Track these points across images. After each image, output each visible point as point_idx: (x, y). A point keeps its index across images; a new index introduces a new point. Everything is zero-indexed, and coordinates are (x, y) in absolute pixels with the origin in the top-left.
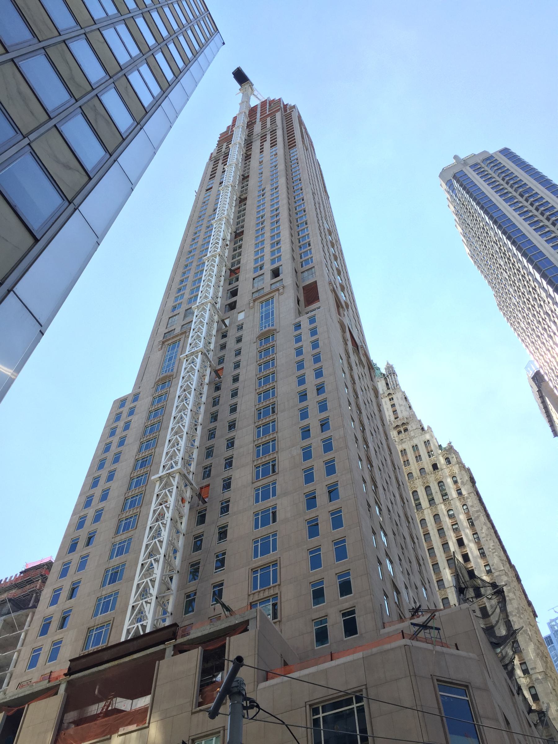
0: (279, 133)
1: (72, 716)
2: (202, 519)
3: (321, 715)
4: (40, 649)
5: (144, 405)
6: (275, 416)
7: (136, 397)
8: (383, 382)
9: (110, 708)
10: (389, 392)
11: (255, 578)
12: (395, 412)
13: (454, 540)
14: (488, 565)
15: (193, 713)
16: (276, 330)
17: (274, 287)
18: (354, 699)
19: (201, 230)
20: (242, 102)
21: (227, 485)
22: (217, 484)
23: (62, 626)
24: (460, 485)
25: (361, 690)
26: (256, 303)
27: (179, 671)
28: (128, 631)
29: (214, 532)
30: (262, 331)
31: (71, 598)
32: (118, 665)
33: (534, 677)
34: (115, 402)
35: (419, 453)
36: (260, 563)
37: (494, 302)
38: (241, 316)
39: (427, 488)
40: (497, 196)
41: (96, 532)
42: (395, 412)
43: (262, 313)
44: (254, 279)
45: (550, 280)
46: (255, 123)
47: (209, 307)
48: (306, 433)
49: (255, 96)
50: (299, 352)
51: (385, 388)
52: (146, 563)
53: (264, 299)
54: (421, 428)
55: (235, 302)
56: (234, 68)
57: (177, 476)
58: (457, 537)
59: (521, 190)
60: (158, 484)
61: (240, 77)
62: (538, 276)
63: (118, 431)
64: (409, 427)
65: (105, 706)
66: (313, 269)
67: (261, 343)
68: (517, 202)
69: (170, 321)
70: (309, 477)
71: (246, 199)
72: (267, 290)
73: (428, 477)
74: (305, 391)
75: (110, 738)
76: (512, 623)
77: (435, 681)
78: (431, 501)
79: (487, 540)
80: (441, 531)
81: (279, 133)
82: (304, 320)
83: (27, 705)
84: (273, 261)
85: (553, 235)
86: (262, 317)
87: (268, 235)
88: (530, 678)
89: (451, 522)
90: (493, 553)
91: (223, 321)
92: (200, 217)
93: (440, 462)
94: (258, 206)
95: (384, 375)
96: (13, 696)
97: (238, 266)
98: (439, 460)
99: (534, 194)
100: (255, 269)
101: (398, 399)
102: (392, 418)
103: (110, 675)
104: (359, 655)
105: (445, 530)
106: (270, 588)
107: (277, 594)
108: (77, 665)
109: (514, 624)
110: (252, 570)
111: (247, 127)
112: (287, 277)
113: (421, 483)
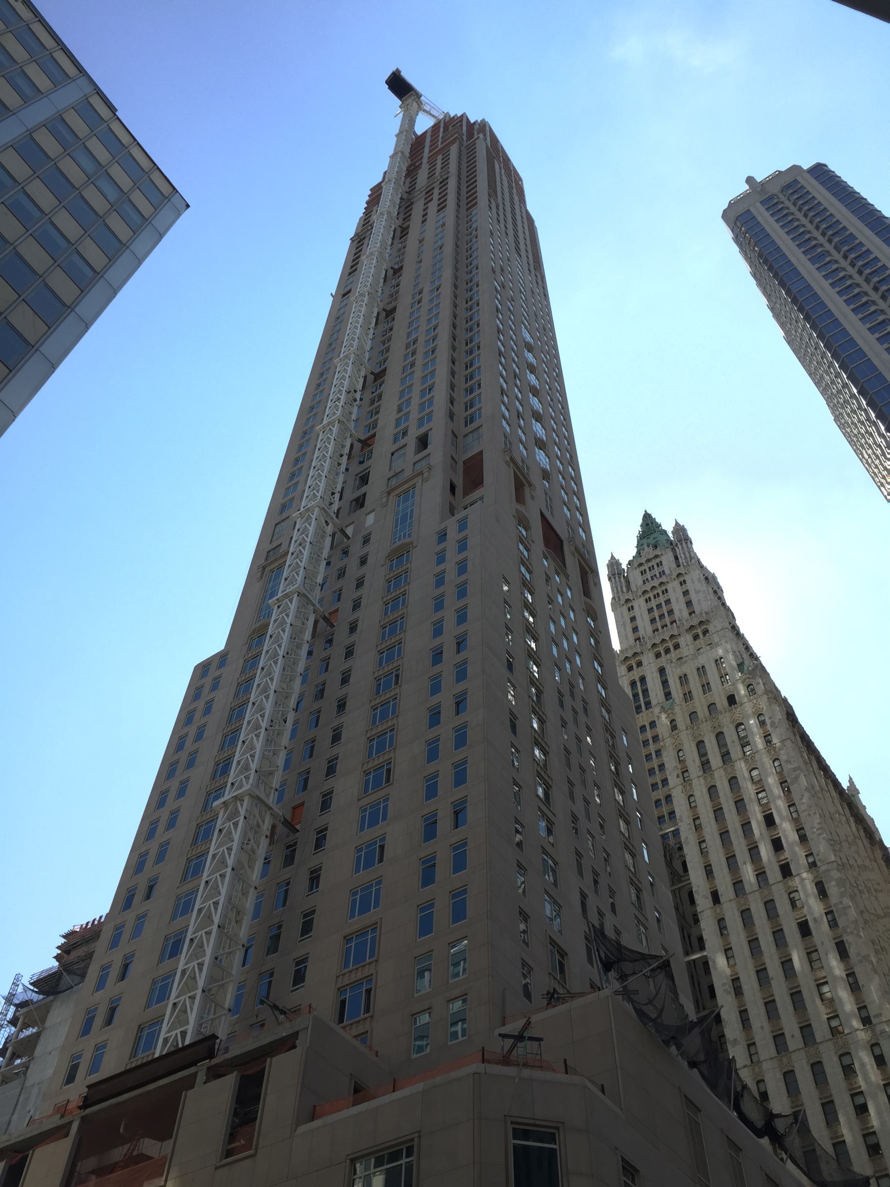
0: (452, 184)
1: (89, 1164)
2: (289, 860)
5: (231, 674)
7: (221, 658)
8: (670, 555)
9: (135, 1153)
11: (348, 950)
12: (689, 603)
13: (760, 817)
15: (216, 1168)
16: (412, 543)
20: (401, 132)
22: (314, 800)
23: (109, 1021)
24: (769, 727)
25: (412, 1140)
26: (391, 497)
27: (208, 1103)
28: (166, 1040)
29: (303, 878)
33: (878, 1028)
35: (707, 678)
38: (370, 520)
39: (720, 736)
40: (799, 252)
41: (157, 878)
42: (689, 603)
43: (397, 514)
44: (392, 454)
45: (871, 398)
48: (435, 717)
50: (440, 581)
51: (674, 565)
53: (402, 489)
56: (387, 74)
57: (246, 800)
59: (836, 239)
61: (399, 85)
63: (197, 715)
64: (711, 628)
65: (129, 1150)
67: (391, 566)
68: (830, 262)
69: (277, 530)
70: (431, 791)
71: (394, 310)
72: (408, 473)
74: (441, 646)
76: (847, 946)
78: (726, 756)
79: (809, 815)
80: (740, 804)
81: (452, 184)
82: (452, 525)
83: (31, 1152)
85: (881, 318)
86: (397, 520)
87: (418, 373)
88: (873, 1031)
89: (755, 788)
90: (819, 834)
91: (343, 532)
93: (738, 693)
95: (671, 543)
97: (373, 431)
98: (737, 689)
99: (857, 244)
101: (693, 582)
102: (685, 613)
104: (419, 1087)
105: (746, 801)
108: (98, 1093)
110: (345, 937)
111: (407, 176)
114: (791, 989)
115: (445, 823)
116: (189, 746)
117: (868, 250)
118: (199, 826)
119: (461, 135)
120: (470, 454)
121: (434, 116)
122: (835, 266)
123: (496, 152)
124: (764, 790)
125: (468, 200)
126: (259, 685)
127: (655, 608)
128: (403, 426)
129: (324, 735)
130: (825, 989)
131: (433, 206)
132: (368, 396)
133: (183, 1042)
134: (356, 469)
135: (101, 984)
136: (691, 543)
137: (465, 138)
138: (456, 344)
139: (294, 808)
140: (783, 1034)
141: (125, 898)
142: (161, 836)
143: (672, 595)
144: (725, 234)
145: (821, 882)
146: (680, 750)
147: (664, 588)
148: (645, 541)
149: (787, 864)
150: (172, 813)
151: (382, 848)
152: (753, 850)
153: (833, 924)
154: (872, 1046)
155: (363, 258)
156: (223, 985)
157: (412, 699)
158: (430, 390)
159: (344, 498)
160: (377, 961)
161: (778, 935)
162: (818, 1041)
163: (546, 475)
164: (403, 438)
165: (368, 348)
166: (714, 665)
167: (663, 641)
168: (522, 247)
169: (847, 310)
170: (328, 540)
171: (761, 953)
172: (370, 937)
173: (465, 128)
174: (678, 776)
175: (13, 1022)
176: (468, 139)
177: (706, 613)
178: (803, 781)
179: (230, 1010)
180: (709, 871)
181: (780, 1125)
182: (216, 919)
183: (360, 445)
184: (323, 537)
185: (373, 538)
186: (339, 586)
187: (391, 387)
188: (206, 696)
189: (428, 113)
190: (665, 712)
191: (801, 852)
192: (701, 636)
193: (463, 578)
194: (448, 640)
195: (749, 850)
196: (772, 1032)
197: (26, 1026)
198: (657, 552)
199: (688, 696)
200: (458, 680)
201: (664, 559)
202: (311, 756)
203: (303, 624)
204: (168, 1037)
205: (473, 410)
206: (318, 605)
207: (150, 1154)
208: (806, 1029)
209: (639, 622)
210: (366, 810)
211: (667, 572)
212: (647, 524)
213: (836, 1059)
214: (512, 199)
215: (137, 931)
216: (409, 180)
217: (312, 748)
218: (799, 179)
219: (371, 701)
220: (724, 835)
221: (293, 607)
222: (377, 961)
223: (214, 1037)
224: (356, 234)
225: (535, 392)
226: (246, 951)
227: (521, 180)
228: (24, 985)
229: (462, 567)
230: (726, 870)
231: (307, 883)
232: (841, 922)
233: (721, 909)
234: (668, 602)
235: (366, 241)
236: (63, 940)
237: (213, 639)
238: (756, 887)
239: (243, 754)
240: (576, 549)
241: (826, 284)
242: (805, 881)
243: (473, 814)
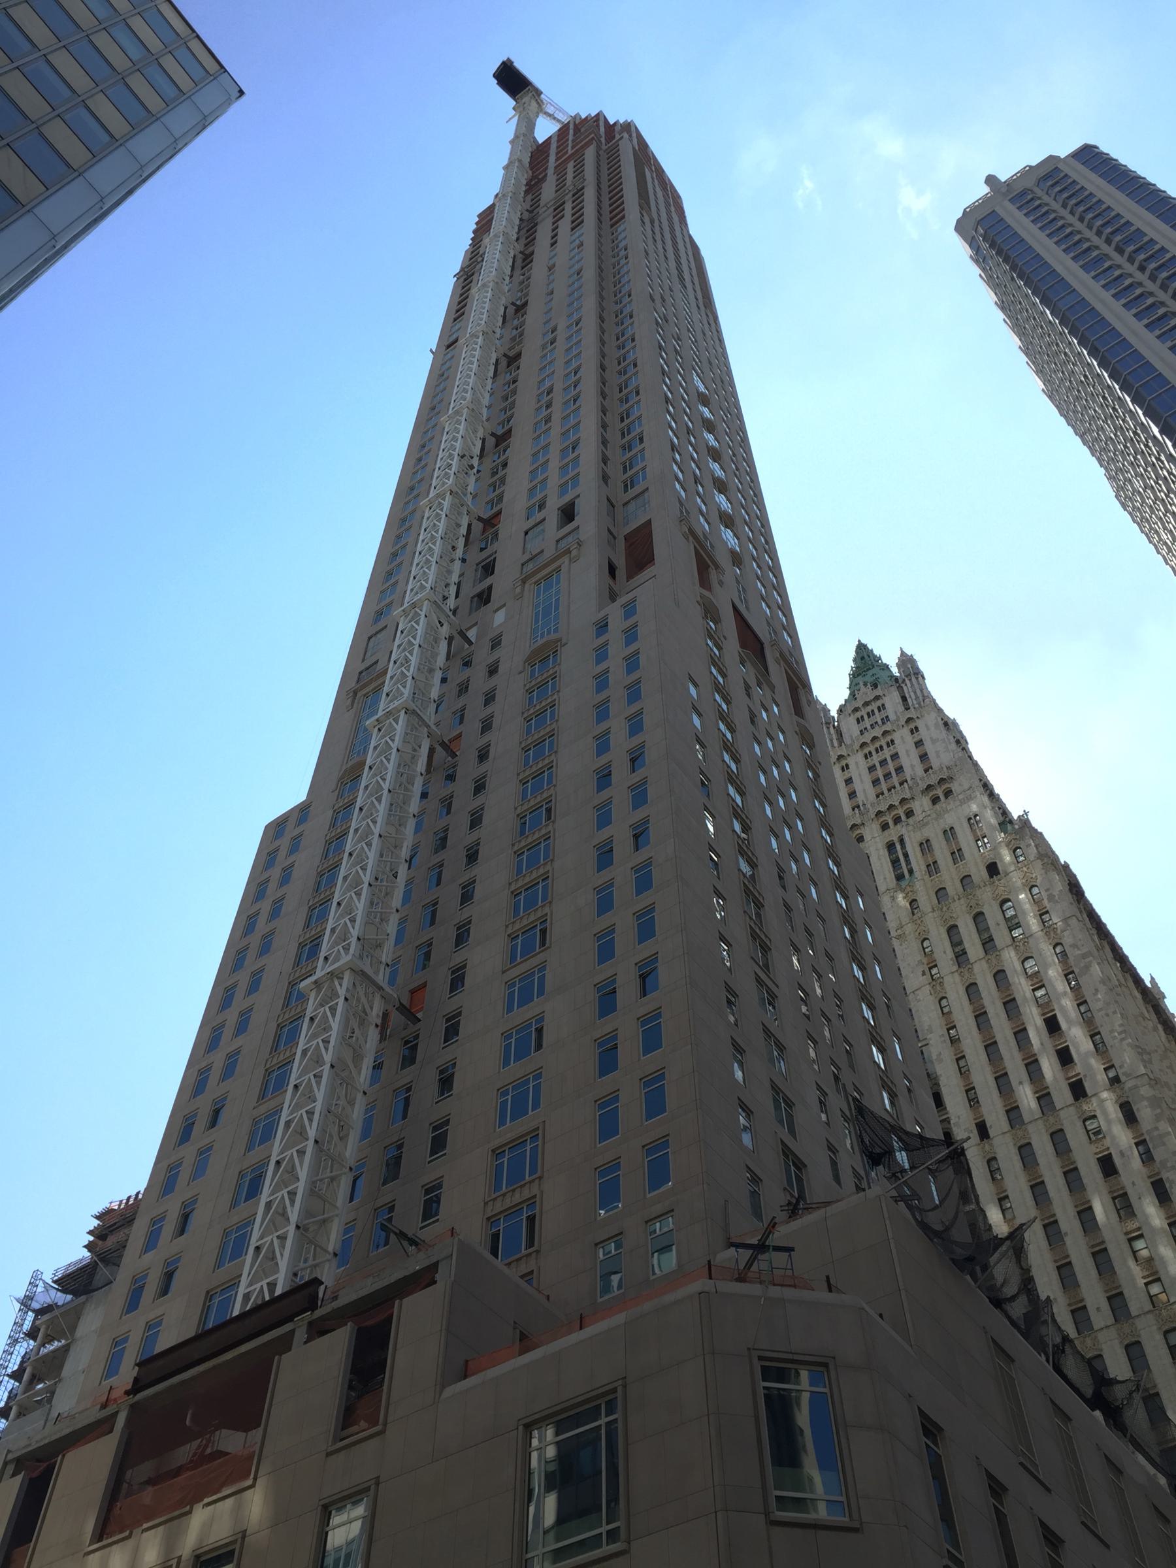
0: (590, 195)
1: (142, 1471)
2: (409, 1059)
4: (126, 1340)
5: (317, 830)
7: (302, 812)
9: (209, 1451)
11: (499, 1168)
12: (924, 757)
13: (1040, 1022)
14: (1113, 1066)
15: (328, 1455)
18: (603, 1407)
20: (516, 137)
21: (457, 980)
22: (440, 978)
23: (165, 1290)
24: (1046, 902)
25: (614, 1390)
26: (527, 586)
27: (312, 1370)
28: (247, 1297)
29: (431, 1078)
30: (537, 645)
32: (214, 1367)
35: (957, 843)
36: (510, 1136)
37: (1106, 490)
38: (500, 618)
39: (978, 917)
40: (1067, 259)
42: (924, 757)
43: (538, 605)
44: (526, 533)
46: (544, 179)
47: (424, 609)
48: (605, 856)
49: (550, 115)
50: (602, 681)
52: (284, 1159)
53: (541, 573)
57: (347, 976)
58: (1043, 1014)
59: (1118, 238)
60: (313, 994)
61: (511, 79)
63: (272, 886)
64: (955, 787)
66: (646, 495)
67: (533, 672)
68: (1110, 267)
69: (371, 645)
70: (606, 951)
71: (519, 355)
72: (549, 553)
73: (978, 892)
74: (609, 765)
75: (190, 1512)
76: (1167, 1185)
77: (755, 1361)
78: (988, 943)
79: (1107, 1015)
81: (590, 195)
82: (614, 612)
84: (563, 488)
86: (537, 614)
90: (1122, 1040)
93: (1002, 860)
94: (567, 363)
95: (896, 680)
97: (498, 508)
101: (928, 729)
102: (919, 770)
104: (619, 1319)
105: (1019, 1001)
106: (524, 1185)
107: (535, 1196)
108: (153, 1368)
109: (1171, 1187)
110: (493, 1151)
111: (527, 192)
113: (964, 908)
114: (1093, 1246)
115: (627, 990)
116: (262, 926)
117: (1163, 248)
118: (280, 1027)
119: (598, 136)
120: (633, 526)
122: (1117, 273)
123: (644, 157)
124: (1043, 986)
125: (613, 213)
126: (345, 878)
127: (878, 765)
128: (539, 496)
129: (450, 894)
130: (1139, 1244)
131: (565, 225)
132: (488, 463)
134: (475, 556)
135: (151, 1242)
136: (923, 678)
137: (603, 140)
138: (606, 390)
139: (413, 992)
140: (1085, 1307)
142: (227, 1045)
143: (900, 748)
144: (961, 251)
145: (1128, 1102)
146: (925, 939)
147: (888, 738)
148: (860, 680)
149: (1080, 1082)
150: (242, 1014)
151: (539, 1031)
152: (1032, 1065)
153: (1147, 1157)
155: (474, 291)
156: (324, 1221)
157: (572, 838)
159: (461, 595)
160: (540, 1178)
161: (1072, 1176)
162: (1133, 1314)
163: (737, 559)
164: (539, 511)
165: (486, 401)
166: (966, 825)
167: (891, 807)
168: (686, 275)
169: (1139, 326)
170: (443, 645)
171: (1048, 1200)
172: (528, 1148)
173: (602, 129)
174: (924, 974)
175: (32, 1334)
176: (608, 142)
177: (948, 768)
178: (1096, 970)
179: (335, 1255)
180: (973, 1100)
181: (1119, 1393)
182: (312, 1133)
183: (481, 525)
184: (436, 640)
185: (505, 640)
186: (460, 705)
187: (520, 450)
188: (282, 860)
189: (551, 116)
190: (903, 890)
191: (1097, 1065)
192: (942, 798)
193: (634, 676)
194: (618, 756)
195: (1026, 1065)
196: (1069, 1305)
197: (49, 1339)
198: (878, 692)
199: (933, 868)
200: (635, 807)
201: (887, 701)
202: (432, 923)
203: (415, 750)
204: (250, 1288)
205: (633, 471)
206: (433, 727)
207: (229, 1451)
208: (1117, 1300)
209: (857, 786)
210: (514, 985)
211: (892, 717)
212: (863, 658)
213: (1159, 1337)
214: (670, 219)
215: (199, 1170)
216: (530, 197)
217: (434, 913)
218: (1060, 166)
219: (513, 845)
220: (991, 1047)
221: (399, 728)
222: (540, 1178)
223: (316, 1282)
224: (462, 269)
225: (715, 455)
226: (354, 1182)
227: (679, 197)
228: (44, 1282)
229: (632, 663)
230: (996, 1092)
231: (435, 1087)
232: (1158, 1154)
233: (991, 1145)
234: (895, 756)
235: (475, 277)
236: (96, 1223)
237: (289, 782)
238: (1038, 1114)
239: (332, 947)
240: (781, 654)
241: (1107, 295)
242: (1106, 1103)
243: (664, 975)
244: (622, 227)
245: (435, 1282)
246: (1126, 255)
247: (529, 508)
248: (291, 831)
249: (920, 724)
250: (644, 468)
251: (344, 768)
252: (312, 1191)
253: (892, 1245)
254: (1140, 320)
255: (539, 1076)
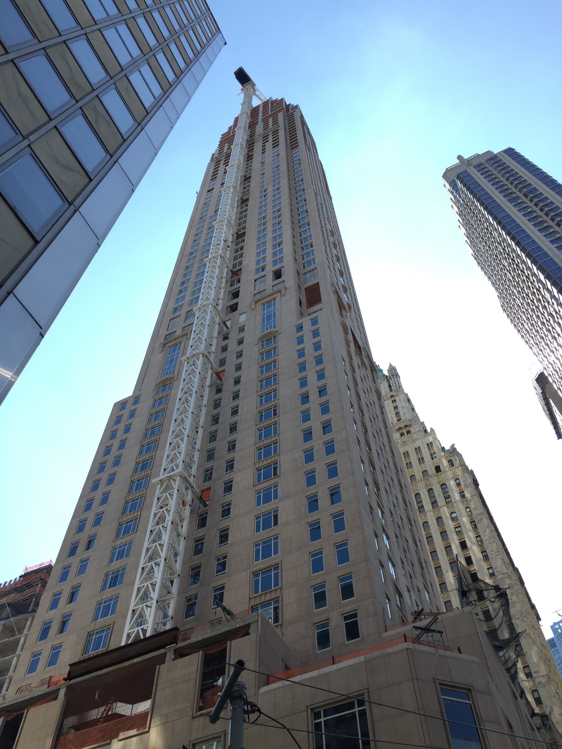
0: (281, 133)
1: (71, 721)
2: (202, 522)
3: (322, 719)
6: (277, 419)
7: (136, 398)
8: (386, 384)
9: (110, 713)
10: (392, 393)
11: (257, 582)
12: (397, 414)
13: (457, 542)
15: (193, 718)
17: (276, 288)
19: (202, 231)
21: (228, 488)
22: (219, 486)
24: (463, 487)
25: (363, 694)
26: (258, 305)
27: (179, 675)
28: (129, 636)
30: (264, 333)
31: (71, 602)
32: (113, 671)
33: (537, 680)
34: (116, 405)
35: (421, 455)
36: (262, 566)
37: (497, 303)
38: (243, 318)
39: (430, 491)
40: (501, 196)
41: (96, 536)
42: (397, 414)
44: (255, 281)
46: (257, 123)
48: (308, 435)
49: (257, 96)
50: (301, 353)
52: (147, 566)
53: (266, 301)
54: (423, 430)
55: (237, 304)
56: (236, 69)
57: (178, 479)
59: (525, 190)
61: (242, 77)
62: (542, 277)
63: (119, 434)
64: (412, 430)
66: (315, 271)
69: (171, 323)
70: (311, 480)
71: (247, 200)
72: (269, 291)
74: (307, 393)
75: (110, 743)
76: (515, 627)
78: (434, 503)
79: (490, 543)
80: (444, 534)
81: (281, 133)
82: (306, 322)
83: (26, 711)
84: (275, 263)
86: (264, 318)
87: (270, 236)
88: (533, 682)
89: (454, 524)
90: (496, 556)
91: (224, 323)
92: (202, 218)
93: (443, 465)
95: (387, 377)
96: (12, 701)
98: (442, 462)
100: (257, 271)
102: (395, 420)
103: (110, 680)
104: (362, 658)
107: (279, 597)
108: (76, 670)
109: (517, 627)
110: (253, 573)
112: (289, 278)
113: (424, 486)
115: (324, 501)
121: (261, 99)
131: (269, 145)
133: (144, 634)
135: (54, 605)
141: (70, 548)
154: (533, 691)
157: (289, 428)
158: (279, 245)
160: (281, 588)
187: (251, 242)
192: (406, 434)
195: (450, 563)
199: (421, 460)
207: (123, 713)
215: (82, 569)
222: (281, 588)
229: (317, 346)
244: (297, 150)
245: (249, 634)
246: (529, 198)
247: (257, 269)
248: (129, 407)
249: (397, 398)
250: (314, 259)
251: (159, 380)
252: (163, 586)
253: (480, 635)
254: (536, 227)
255: (277, 538)
